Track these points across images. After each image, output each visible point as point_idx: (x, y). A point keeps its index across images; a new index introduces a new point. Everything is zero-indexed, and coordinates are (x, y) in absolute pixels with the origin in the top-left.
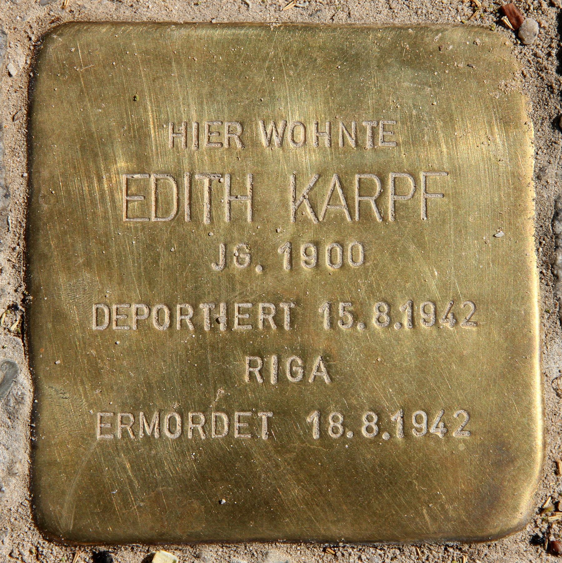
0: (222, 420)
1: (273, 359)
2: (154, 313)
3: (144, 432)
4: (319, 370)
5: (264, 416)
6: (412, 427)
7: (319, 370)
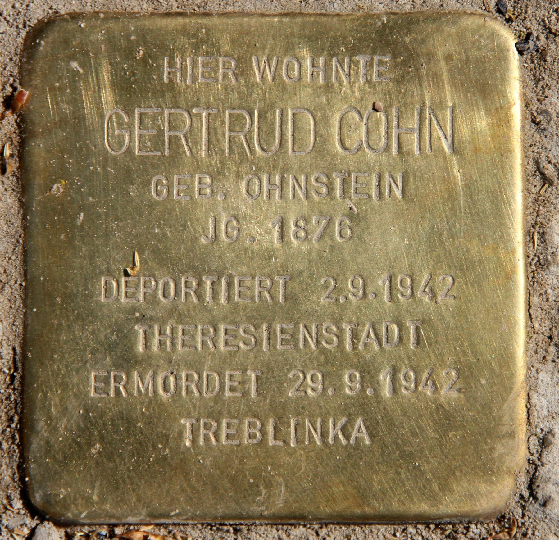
6: (400, 385)
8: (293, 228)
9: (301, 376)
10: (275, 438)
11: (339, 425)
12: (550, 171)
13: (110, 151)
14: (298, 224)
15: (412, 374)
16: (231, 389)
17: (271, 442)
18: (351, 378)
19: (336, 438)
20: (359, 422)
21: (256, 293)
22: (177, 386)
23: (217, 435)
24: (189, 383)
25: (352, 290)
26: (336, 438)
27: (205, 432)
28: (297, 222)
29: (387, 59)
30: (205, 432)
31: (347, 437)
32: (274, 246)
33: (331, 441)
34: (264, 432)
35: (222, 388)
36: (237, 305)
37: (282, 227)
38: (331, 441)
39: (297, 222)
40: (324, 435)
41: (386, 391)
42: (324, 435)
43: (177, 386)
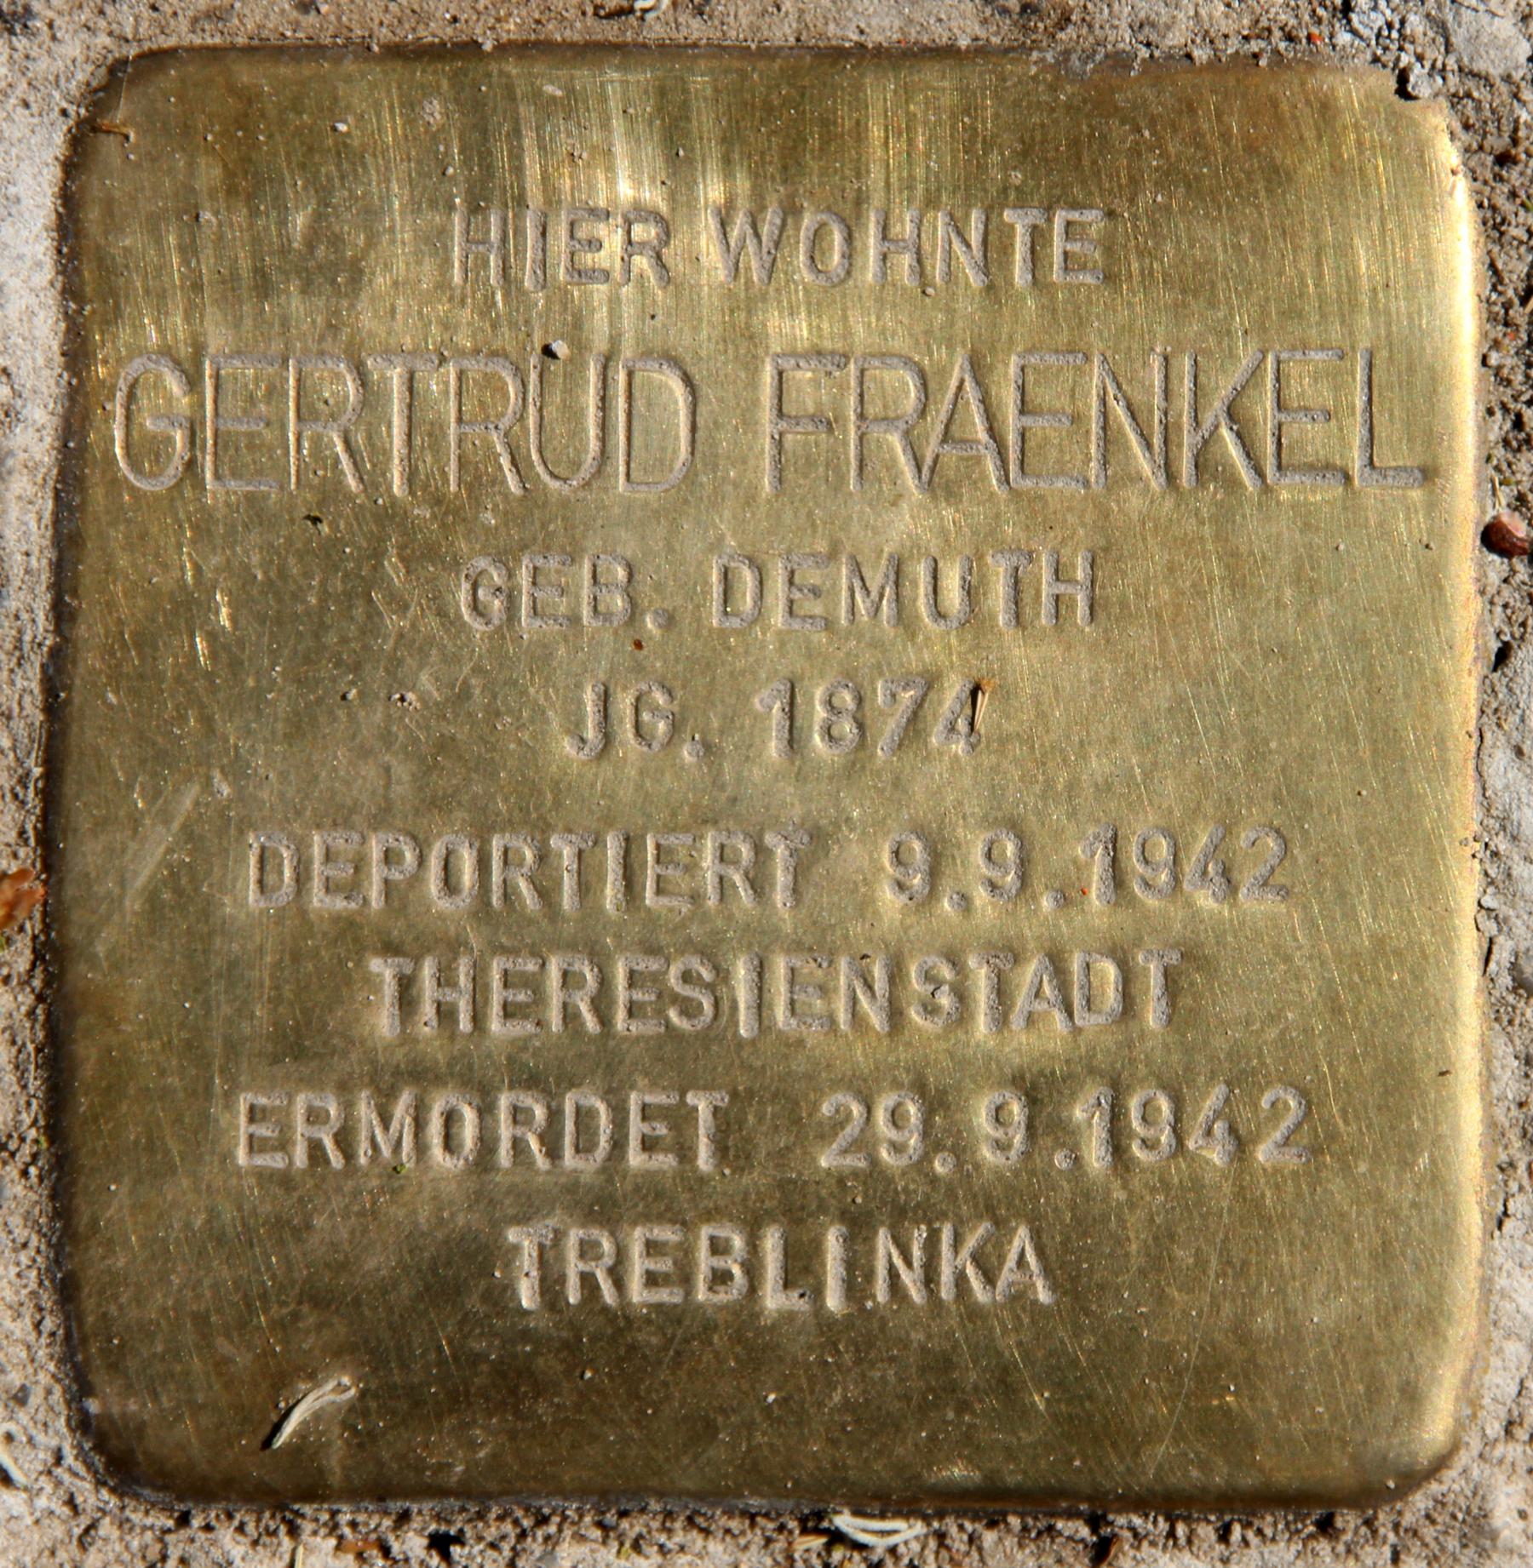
1: (742, 972)
3: (374, 1145)
6: (1131, 1134)
8: (820, 713)
9: (856, 1109)
10: (787, 1284)
11: (971, 1242)
12: (4, 379)
13: (122, 464)
14: (835, 701)
15: (1165, 1105)
16: (649, 1145)
17: (774, 1300)
18: (999, 1115)
19: (961, 1279)
20: (1021, 1238)
21: (710, 879)
22: (487, 1144)
23: (617, 1276)
24: (519, 1132)
25: (985, 870)
26: (961, 1279)
27: (582, 1266)
28: (831, 696)
29: (1092, 217)
30: (582, 1266)
31: (990, 1279)
32: (1328, 1548)
33: (946, 1292)
34: (753, 1269)
35: (618, 1144)
36: (651, 919)
37: (791, 712)
38: (946, 1292)
39: (831, 696)
40: (930, 1278)
41: (1096, 1156)
42: (930, 1278)
43: (487, 1144)
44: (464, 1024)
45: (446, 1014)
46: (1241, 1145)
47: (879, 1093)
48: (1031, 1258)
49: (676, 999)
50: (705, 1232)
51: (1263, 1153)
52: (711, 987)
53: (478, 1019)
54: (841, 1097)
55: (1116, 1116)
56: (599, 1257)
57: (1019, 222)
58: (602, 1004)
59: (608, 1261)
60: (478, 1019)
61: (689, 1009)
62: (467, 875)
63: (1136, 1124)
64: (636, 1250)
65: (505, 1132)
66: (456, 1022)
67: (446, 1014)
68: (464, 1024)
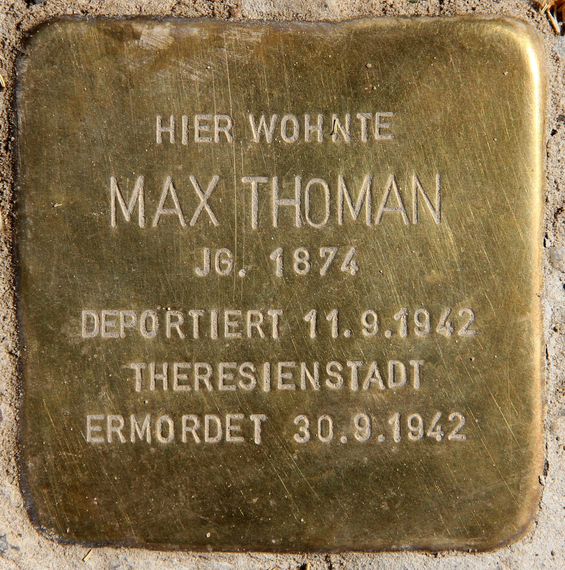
0: (216, 424)
2: (142, 322)
3: (136, 433)
4: (373, 375)
5: (256, 419)
6: (414, 325)
7: (373, 375)
41: (402, 333)
44: (165, 388)
45: (158, 384)
46: (455, 326)
47: (338, 50)
48: (377, 373)
49: (242, 378)
50: (249, 313)
51: (461, 332)
52: (254, 374)
53: (170, 385)
54: (300, 417)
55: (409, 319)
56: (205, 374)
57: (362, 117)
58: (213, 380)
59: (209, 374)
60: (170, 385)
61: (247, 381)
62: (154, 326)
63: (416, 321)
64: (220, 370)
65: (184, 429)
66: (162, 387)
67: (158, 384)
68: (165, 388)
